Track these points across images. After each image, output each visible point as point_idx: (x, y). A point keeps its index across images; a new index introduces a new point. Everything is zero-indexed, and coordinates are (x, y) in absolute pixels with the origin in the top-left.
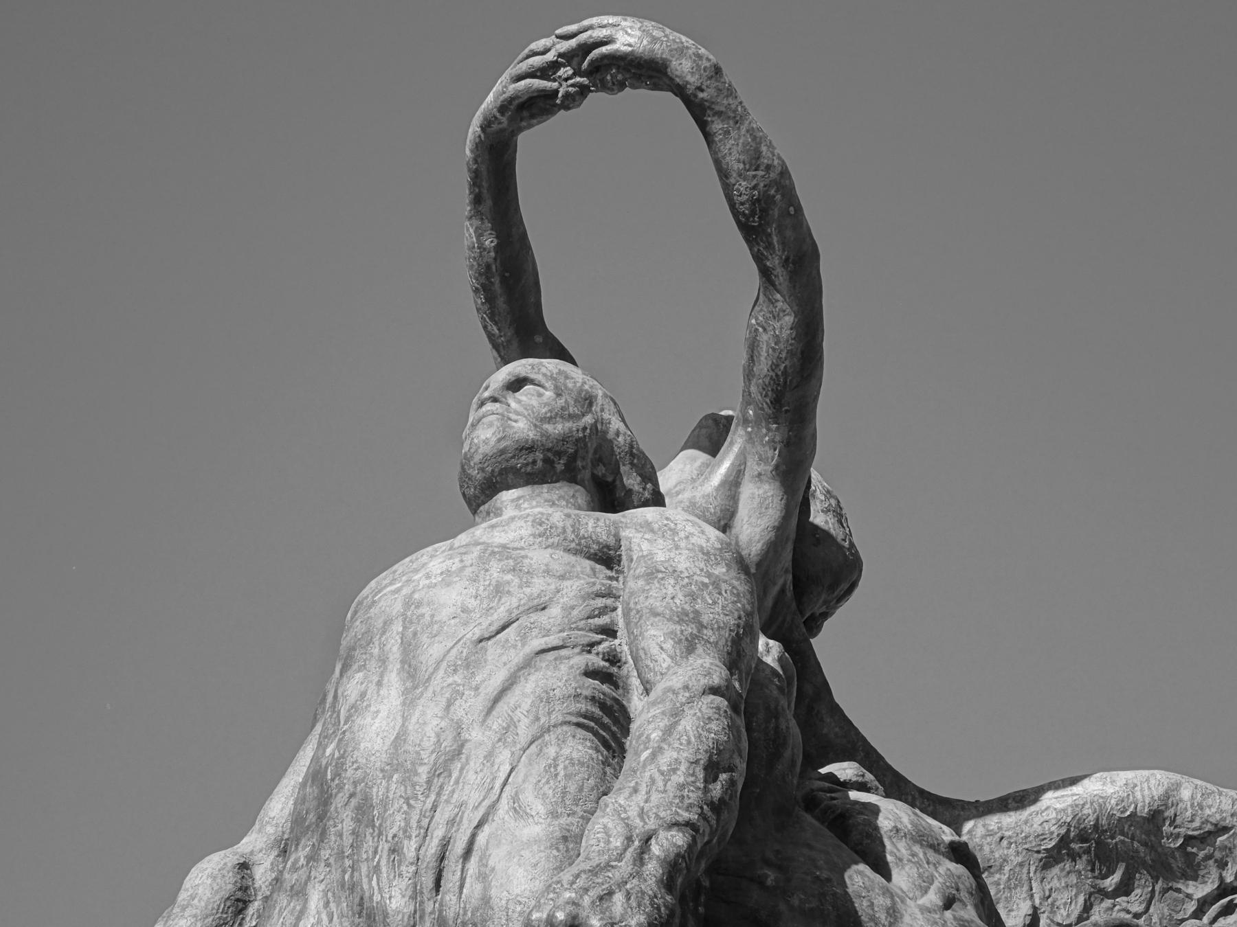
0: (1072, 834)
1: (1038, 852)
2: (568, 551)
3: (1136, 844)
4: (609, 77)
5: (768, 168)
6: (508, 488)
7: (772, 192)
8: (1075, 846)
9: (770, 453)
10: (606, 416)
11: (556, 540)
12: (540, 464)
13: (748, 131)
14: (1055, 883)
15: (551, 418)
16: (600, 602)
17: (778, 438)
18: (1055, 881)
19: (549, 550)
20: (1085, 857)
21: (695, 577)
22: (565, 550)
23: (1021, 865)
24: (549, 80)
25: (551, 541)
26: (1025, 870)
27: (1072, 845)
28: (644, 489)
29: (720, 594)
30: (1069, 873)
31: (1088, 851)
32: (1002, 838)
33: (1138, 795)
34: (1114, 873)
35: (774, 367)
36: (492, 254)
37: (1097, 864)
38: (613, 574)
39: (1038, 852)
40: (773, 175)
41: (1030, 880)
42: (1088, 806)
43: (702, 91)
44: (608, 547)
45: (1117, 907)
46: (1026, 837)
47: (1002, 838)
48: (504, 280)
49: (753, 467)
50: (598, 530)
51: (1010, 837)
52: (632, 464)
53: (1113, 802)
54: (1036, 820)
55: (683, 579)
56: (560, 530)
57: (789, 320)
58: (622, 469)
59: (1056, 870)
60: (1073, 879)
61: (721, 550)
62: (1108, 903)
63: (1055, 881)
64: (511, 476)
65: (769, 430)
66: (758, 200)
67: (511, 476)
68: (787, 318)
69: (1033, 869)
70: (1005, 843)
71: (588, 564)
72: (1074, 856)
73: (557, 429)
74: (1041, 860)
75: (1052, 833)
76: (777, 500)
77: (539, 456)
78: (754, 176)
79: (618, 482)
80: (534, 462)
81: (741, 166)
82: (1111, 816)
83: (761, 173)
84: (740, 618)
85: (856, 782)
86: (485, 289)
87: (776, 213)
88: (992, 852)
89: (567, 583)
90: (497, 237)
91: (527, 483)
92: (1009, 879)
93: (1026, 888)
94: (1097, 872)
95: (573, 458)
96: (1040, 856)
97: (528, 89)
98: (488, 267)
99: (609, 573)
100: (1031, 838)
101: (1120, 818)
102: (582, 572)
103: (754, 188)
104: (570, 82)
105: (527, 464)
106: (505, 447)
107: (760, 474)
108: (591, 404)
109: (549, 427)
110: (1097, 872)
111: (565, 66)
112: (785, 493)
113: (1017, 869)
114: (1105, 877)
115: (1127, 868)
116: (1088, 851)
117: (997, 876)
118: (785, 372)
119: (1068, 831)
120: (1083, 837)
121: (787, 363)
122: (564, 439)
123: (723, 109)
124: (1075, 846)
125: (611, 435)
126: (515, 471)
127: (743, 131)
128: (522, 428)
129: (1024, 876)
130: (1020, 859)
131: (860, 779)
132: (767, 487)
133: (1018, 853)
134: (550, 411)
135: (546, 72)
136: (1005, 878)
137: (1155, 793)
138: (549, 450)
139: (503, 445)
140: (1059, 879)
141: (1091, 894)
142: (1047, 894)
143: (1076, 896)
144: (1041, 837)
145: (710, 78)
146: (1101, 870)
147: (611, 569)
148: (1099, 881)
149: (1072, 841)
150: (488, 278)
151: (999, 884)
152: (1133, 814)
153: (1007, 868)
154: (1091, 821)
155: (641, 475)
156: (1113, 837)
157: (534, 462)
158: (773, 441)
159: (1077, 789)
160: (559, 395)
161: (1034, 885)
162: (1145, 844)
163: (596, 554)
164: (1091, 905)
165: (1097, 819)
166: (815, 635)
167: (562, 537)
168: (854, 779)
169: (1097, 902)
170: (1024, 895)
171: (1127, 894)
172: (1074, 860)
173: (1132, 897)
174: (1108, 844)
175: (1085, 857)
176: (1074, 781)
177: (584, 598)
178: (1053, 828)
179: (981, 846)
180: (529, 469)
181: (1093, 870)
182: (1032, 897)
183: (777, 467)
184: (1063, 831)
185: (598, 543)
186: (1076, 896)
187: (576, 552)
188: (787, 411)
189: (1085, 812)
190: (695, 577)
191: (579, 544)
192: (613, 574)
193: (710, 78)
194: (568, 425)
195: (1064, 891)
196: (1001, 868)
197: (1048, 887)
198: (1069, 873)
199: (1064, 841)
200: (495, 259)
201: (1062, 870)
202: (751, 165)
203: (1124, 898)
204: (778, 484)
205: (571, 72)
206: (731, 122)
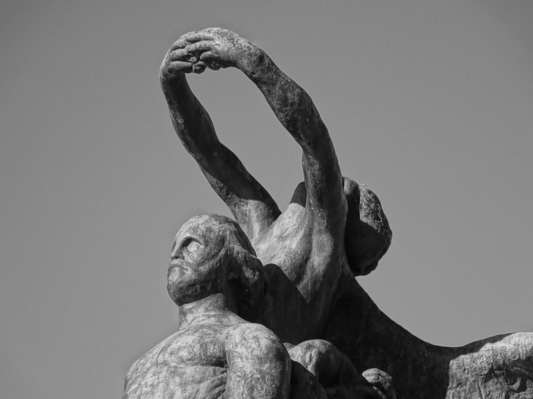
0: (494, 368)
1: (481, 375)
2: (202, 365)
3: (523, 371)
4: (212, 65)
5: (292, 104)
6: (187, 303)
7: (296, 116)
8: (497, 372)
9: (322, 221)
10: (231, 246)
11: (197, 361)
12: (199, 290)
13: (279, 88)
14: (491, 388)
15: (203, 262)
16: (217, 390)
17: (324, 215)
18: (491, 387)
19: (195, 366)
20: (502, 377)
21: (255, 376)
22: (201, 365)
23: (474, 381)
24: (187, 61)
25: (194, 362)
26: (477, 384)
27: (496, 372)
28: (254, 276)
29: (265, 382)
30: (496, 383)
31: (503, 374)
32: (465, 369)
33: (520, 350)
34: (516, 382)
35: (315, 186)
36: (183, 126)
37: (508, 379)
38: (225, 369)
39: (481, 375)
40: (295, 107)
41: (479, 388)
42: (499, 355)
43: (255, 74)
44: (220, 358)
45: (521, 397)
46: (475, 369)
47: (465, 369)
48: (191, 136)
49: (316, 228)
50: (215, 350)
51: (468, 369)
52: (247, 265)
53: (509, 354)
54: (478, 361)
55: (248, 378)
56: (198, 355)
57: (317, 166)
58: (243, 268)
59: (490, 382)
60: (499, 386)
61: (267, 354)
62: (516, 395)
63: (491, 387)
64: (187, 298)
65: (319, 211)
66: (290, 121)
67: (187, 298)
68: (316, 166)
69: (480, 383)
70: (466, 371)
71: (211, 368)
72: (497, 376)
73: (204, 269)
74: (483, 379)
75: (485, 367)
76: (329, 242)
77: (198, 286)
78: (286, 110)
79: (241, 276)
80: (196, 290)
81: (279, 106)
82: (509, 360)
83: (288, 108)
84: (273, 394)
85: (375, 383)
86: (182, 134)
87: (299, 124)
88: (461, 376)
89: (202, 385)
90: (183, 118)
91: (195, 300)
92: (470, 388)
93: (478, 392)
94: (509, 383)
95: (215, 280)
96: (483, 377)
97: (178, 66)
98: (182, 131)
99: (222, 369)
100: (477, 369)
101: (514, 361)
102: (209, 375)
103: (287, 115)
104: (196, 64)
105: (193, 292)
106: (182, 287)
107: (320, 230)
108: (224, 243)
109: (202, 268)
110: (509, 383)
111: (193, 57)
112: (333, 237)
113: (473, 383)
114: (514, 384)
115: (522, 380)
116: (503, 374)
117: (465, 387)
118: (320, 189)
119: (492, 366)
120: (499, 368)
121: (320, 185)
122: (210, 272)
123: (266, 80)
124: (497, 372)
125: (235, 255)
126: (189, 296)
127: (277, 88)
128: (189, 274)
129: (477, 387)
130: (474, 379)
131: (377, 381)
132: (324, 236)
133: (472, 376)
134: (202, 258)
135: (184, 58)
136: (468, 388)
137: (528, 349)
138: (203, 282)
139: (181, 285)
140: (493, 386)
141: (508, 392)
142: (488, 393)
143: (501, 393)
144: (481, 369)
145: (257, 66)
146: (510, 382)
147: (223, 367)
148: (510, 386)
149: (495, 370)
150: (183, 136)
151: (466, 391)
152: (519, 359)
153: (468, 384)
154: (501, 362)
155: (251, 269)
156: (512, 368)
157: (196, 290)
158: (322, 216)
159: (499, 345)
160: (206, 246)
161: (482, 390)
162: (527, 370)
163: (215, 363)
164: (509, 397)
165: (504, 361)
166: (366, 272)
167: (199, 359)
168: (374, 382)
169: (511, 395)
170: (477, 395)
171: (524, 390)
172: (498, 378)
173: (527, 392)
174: (511, 371)
175: (502, 377)
176: (500, 338)
177: (209, 391)
178: (486, 365)
179: (456, 374)
180: (194, 294)
181: (507, 382)
182: (481, 395)
183: (327, 227)
184: (490, 367)
185: (216, 357)
186: (501, 393)
187: (206, 364)
188: (325, 204)
189: (498, 358)
190: (255, 376)
191: (207, 361)
192: (225, 369)
193: (257, 66)
194: (211, 263)
195: (496, 391)
196: (466, 384)
197: (488, 390)
198: (496, 383)
199: (491, 370)
200: (185, 128)
201: (493, 382)
202: (283, 105)
203: (523, 392)
204: (329, 234)
205: (195, 60)
206: (271, 86)
